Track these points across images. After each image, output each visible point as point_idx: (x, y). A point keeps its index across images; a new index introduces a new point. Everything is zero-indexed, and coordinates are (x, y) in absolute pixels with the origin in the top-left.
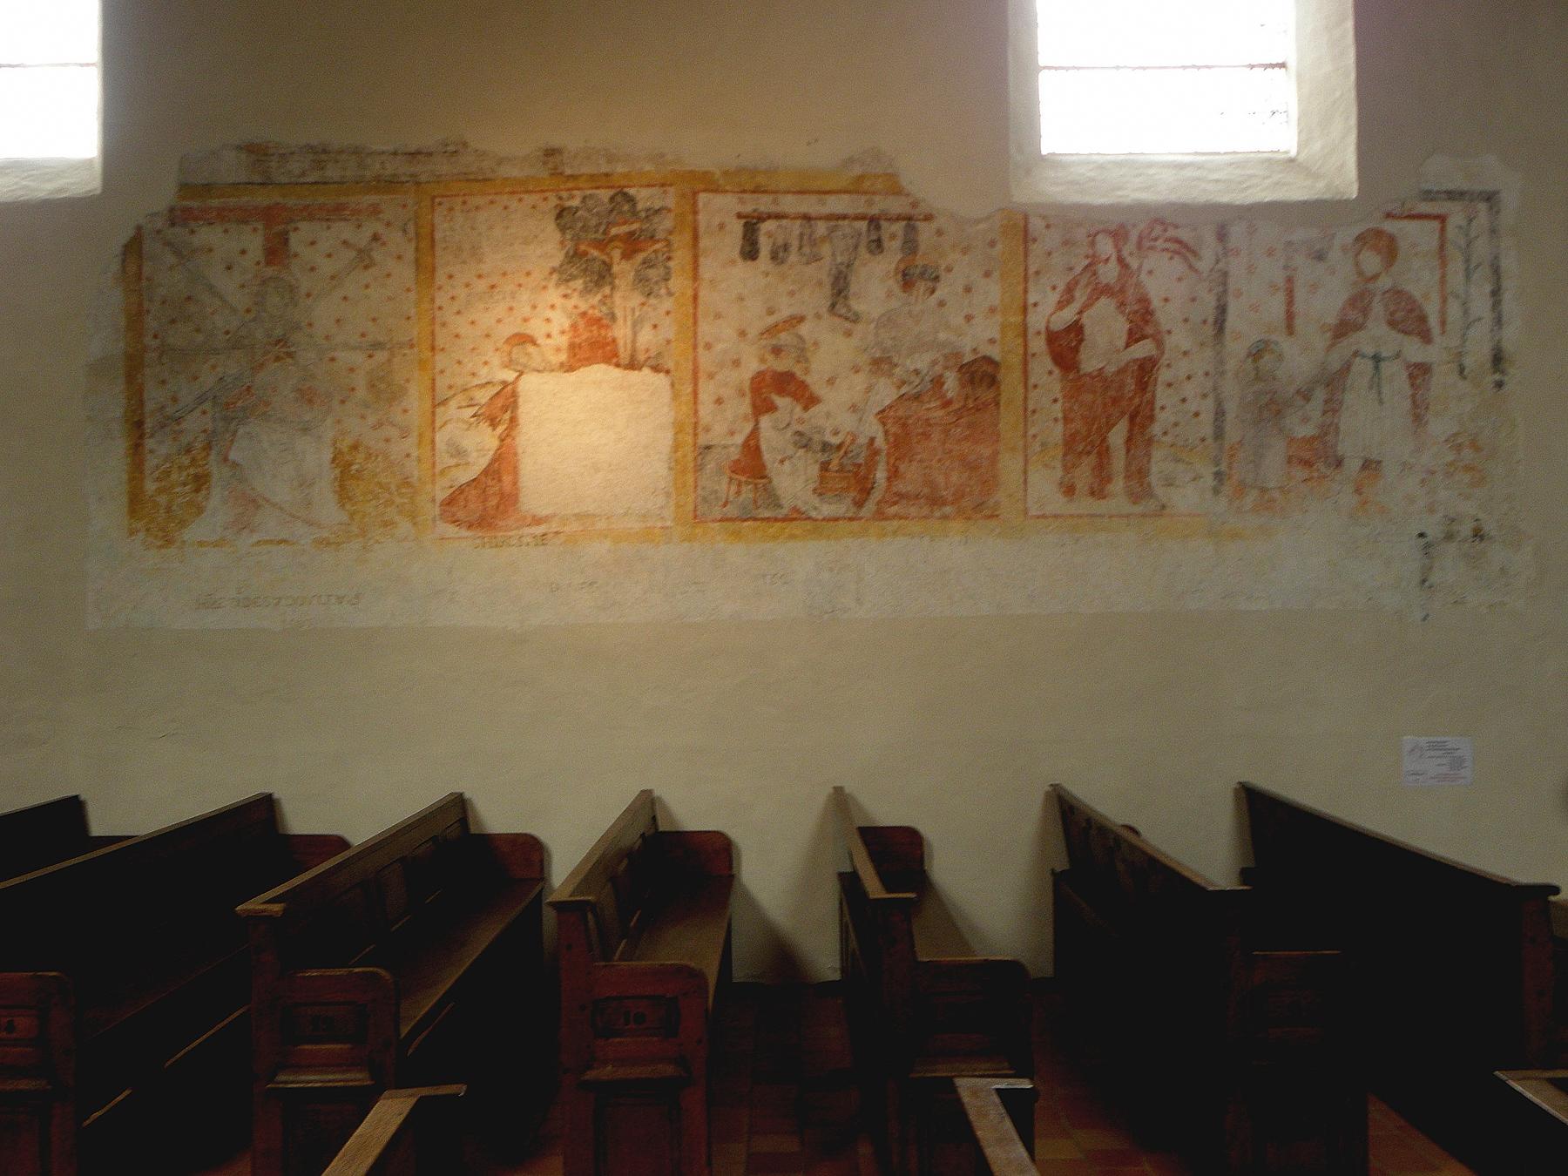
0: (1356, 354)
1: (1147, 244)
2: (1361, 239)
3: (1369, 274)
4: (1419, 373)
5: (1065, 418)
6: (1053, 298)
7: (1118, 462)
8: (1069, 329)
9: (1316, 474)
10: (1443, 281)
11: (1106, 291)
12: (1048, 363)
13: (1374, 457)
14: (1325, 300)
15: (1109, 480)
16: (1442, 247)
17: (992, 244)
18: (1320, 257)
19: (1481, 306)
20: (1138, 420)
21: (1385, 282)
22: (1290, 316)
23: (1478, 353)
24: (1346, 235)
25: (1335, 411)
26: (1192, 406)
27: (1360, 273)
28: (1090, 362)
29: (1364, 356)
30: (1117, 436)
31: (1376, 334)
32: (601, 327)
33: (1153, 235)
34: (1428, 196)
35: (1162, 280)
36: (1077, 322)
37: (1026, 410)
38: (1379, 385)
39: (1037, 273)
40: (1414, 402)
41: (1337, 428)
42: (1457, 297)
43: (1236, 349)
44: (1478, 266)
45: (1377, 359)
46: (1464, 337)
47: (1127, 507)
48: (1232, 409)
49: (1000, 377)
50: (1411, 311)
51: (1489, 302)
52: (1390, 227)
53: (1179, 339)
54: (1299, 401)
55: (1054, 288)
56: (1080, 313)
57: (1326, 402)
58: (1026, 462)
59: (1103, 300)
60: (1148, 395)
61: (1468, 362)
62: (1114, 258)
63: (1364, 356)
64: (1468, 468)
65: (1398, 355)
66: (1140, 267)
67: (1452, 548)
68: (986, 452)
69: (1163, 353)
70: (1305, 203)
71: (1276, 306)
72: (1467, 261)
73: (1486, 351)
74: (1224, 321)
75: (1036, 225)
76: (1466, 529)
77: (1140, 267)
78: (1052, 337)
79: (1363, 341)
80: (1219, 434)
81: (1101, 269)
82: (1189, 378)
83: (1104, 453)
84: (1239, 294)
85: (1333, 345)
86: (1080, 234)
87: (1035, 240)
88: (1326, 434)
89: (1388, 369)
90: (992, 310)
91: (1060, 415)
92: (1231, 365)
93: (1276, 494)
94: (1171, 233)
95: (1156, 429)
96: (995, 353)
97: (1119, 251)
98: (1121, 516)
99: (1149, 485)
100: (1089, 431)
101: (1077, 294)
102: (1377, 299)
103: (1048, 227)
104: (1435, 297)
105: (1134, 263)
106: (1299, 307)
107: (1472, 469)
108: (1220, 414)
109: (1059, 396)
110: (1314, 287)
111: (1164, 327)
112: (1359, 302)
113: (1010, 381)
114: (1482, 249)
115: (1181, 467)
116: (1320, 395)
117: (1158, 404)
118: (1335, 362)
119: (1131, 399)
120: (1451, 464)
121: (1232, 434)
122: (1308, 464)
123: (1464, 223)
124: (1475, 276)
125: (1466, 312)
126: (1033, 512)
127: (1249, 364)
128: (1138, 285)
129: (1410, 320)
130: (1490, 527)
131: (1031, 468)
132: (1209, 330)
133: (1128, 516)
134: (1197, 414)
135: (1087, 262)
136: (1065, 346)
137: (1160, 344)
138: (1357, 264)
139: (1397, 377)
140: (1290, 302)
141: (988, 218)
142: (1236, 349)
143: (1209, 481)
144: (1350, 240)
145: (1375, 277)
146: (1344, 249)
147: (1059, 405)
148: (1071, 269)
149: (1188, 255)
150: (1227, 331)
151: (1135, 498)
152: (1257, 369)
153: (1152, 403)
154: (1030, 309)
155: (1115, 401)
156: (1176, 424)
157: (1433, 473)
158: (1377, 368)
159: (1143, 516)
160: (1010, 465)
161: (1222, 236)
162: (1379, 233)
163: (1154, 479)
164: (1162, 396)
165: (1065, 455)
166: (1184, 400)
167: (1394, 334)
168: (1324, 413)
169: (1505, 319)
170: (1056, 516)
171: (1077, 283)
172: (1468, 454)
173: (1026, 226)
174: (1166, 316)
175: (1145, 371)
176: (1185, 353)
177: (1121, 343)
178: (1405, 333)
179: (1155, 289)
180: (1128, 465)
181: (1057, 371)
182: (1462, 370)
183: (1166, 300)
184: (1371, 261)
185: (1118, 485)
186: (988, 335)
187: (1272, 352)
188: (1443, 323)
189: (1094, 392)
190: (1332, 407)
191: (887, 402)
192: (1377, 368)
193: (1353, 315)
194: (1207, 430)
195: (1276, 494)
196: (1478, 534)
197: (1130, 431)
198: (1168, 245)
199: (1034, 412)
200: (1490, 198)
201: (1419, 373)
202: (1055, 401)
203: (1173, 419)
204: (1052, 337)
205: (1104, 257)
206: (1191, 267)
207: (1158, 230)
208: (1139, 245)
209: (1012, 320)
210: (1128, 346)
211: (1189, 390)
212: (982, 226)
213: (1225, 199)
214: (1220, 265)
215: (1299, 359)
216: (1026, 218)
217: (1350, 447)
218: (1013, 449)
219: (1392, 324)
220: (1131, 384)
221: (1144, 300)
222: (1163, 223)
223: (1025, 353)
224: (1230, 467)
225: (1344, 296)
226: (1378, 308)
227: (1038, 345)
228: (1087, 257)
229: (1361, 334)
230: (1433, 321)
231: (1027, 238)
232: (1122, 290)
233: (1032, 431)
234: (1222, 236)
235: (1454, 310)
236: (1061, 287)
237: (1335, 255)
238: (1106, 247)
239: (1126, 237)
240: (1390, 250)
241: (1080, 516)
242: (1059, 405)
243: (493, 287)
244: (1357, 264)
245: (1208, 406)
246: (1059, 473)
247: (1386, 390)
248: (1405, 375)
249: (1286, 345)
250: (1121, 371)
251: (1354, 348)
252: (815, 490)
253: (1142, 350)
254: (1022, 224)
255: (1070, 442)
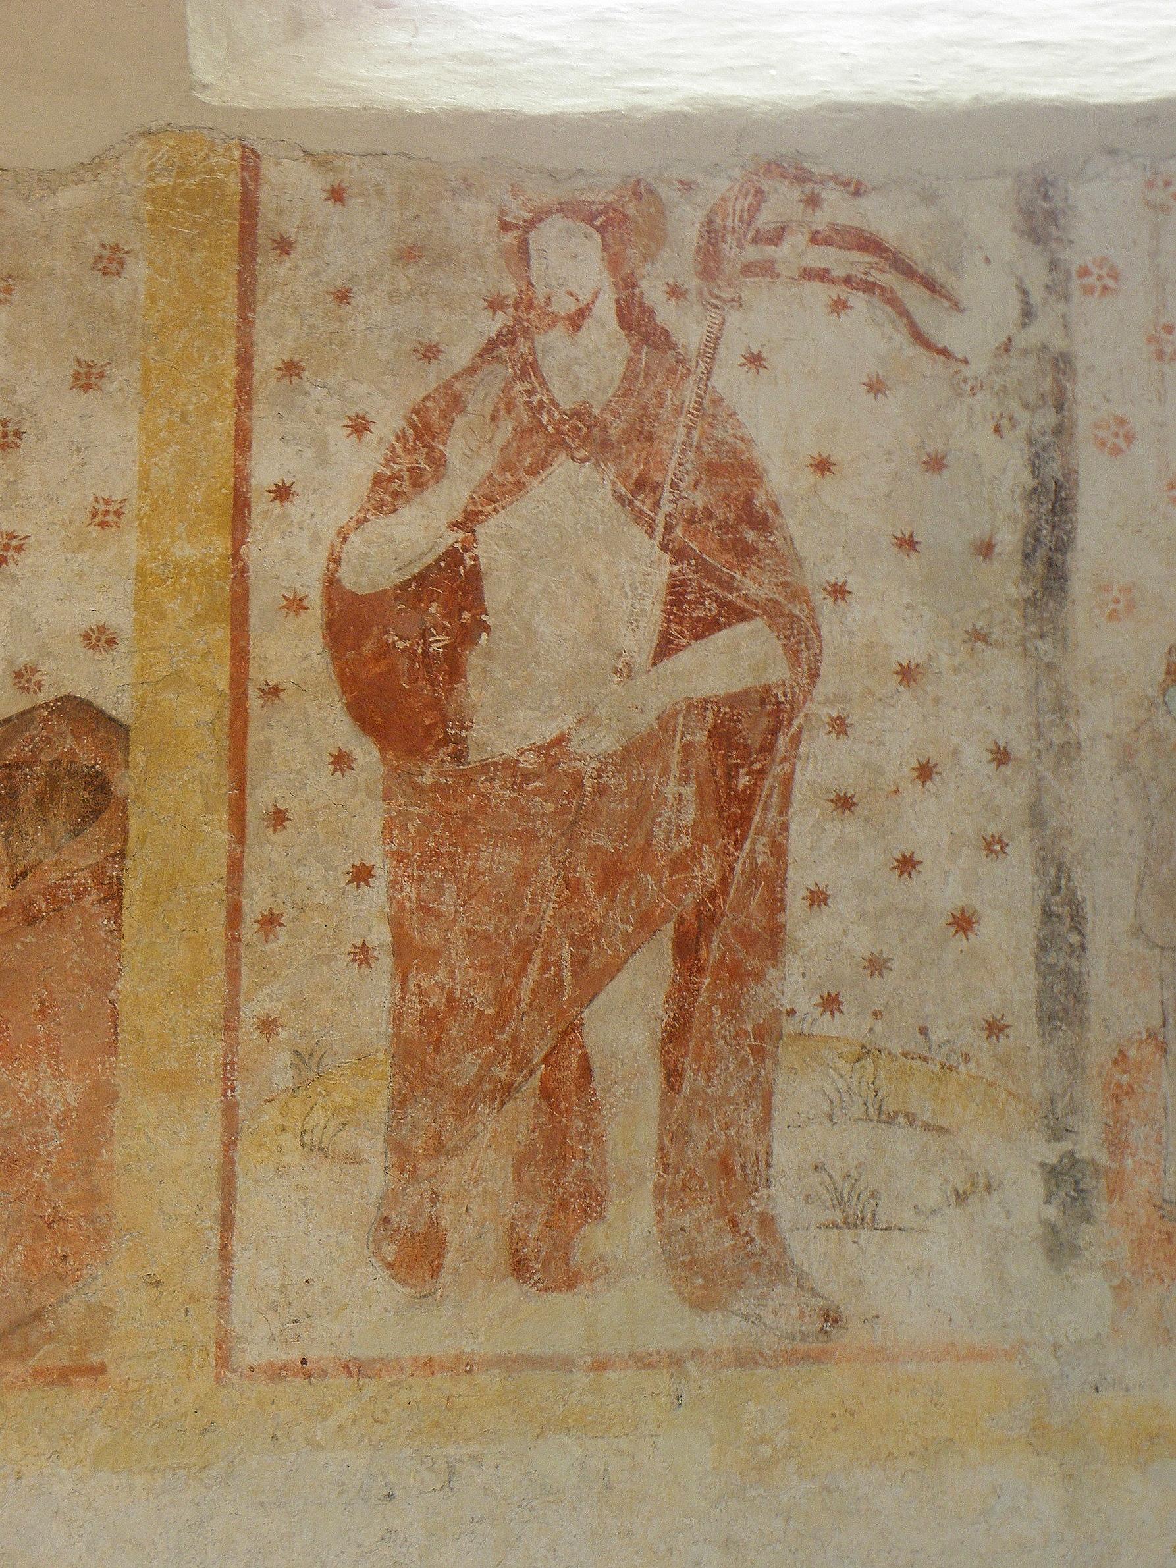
1: (735, 253)
5: (401, 947)
7: (631, 1124)
11: (580, 434)
12: (336, 726)
15: (592, 1202)
17: (111, 262)
20: (712, 952)
26: (943, 888)
28: (506, 712)
30: (625, 1021)
32: (508, 411)
33: (765, 219)
35: (798, 388)
36: (453, 556)
37: (235, 915)
39: (291, 369)
47: (672, 1325)
49: (123, 784)
53: (878, 617)
55: (359, 426)
56: (468, 522)
58: (230, 1143)
59: (562, 469)
60: (757, 846)
62: (605, 308)
66: (715, 340)
68: (62, 1094)
69: (814, 676)
74: (1062, 546)
75: (290, 186)
78: (349, 621)
80: (1062, 1001)
81: (555, 349)
82: (925, 772)
83: (567, 1087)
86: (471, 222)
87: (284, 246)
90: (105, 516)
91: (380, 936)
92: (1101, 717)
94: (838, 209)
95: (792, 986)
96: (110, 685)
97: (629, 284)
98: (644, 1362)
99: (767, 1222)
100: (504, 999)
101: (455, 449)
103: (337, 195)
105: (688, 328)
108: (1061, 918)
109: (377, 857)
111: (817, 573)
113: (171, 802)
115: (903, 1143)
117: (799, 881)
119: (680, 864)
126: (256, 1349)
128: (709, 409)
131: (245, 1154)
132: (1006, 582)
133: (675, 1361)
134: (963, 923)
135: (495, 324)
136: (405, 658)
137: (800, 639)
141: (94, 166)
143: (1027, 1202)
147: (377, 892)
148: (430, 353)
149: (912, 295)
150: (1080, 585)
151: (704, 1281)
153: (771, 882)
154: (260, 505)
155: (612, 874)
156: (876, 965)
159: (746, 1359)
160: (161, 1149)
161: (1041, 217)
163: (786, 1199)
164: (815, 850)
165: (400, 1102)
166: (907, 864)
170: (355, 1369)
171: (456, 403)
173: (249, 208)
174: (823, 530)
175: (741, 750)
176: (907, 674)
177: (638, 641)
179: (774, 425)
180: (674, 1135)
181: (367, 754)
183: (823, 466)
185: (630, 1227)
186: (82, 616)
189: (527, 838)
194: (1012, 985)
197: (682, 998)
198: (818, 257)
199: (270, 921)
202: (362, 875)
203: (862, 943)
204: (349, 621)
205: (563, 305)
206: (919, 338)
207: (783, 201)
209: (184, 551)
210: (666, 648)
211: (927, 822)
212: (65, 198)
214: (1037, 332)
216: (250, 162)
218: (175, 1083)
220: (680, 803)
221: (734, 469)
222: (802, 177)
223: (239, 683)
227: (293, 651)
228: (495, 305)
231: (252, 236)
232: (642, 433)
233: (253, 1008)
234: (1041, 217)
236: (388, 422)
238: (573, 266)
239: (656, 235)
241: (466, 1367)
242: (377, 892)
245: (1014, 883)
246: (376, 1178)
250: (640, 750)
254: (233, 185)
255: (418, 1053)
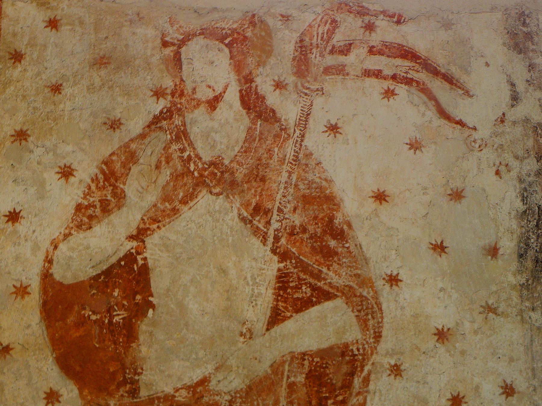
1: (318, 60)
6: (65, 197)
8: (106, 278)
11: (216, 177)
33: (338, 39)
36: (130, 258)
53: (421, 298)
56: (140, 235)
59: (204, 200)
62: (233, 96)
66: (306, 116)
69: (378, 336)
77: (306, 116)
78: (58, 301)
81: (199, 122)
94: (386, 32)
97: (248, 80)
101: (131, 187)
103: (53, 24)
105: (288, 109)
111: (379, 267)
128: (302, 160)
135: (158, 106)
137: (368, 312)
148: (115, 125)
149: (437, 86)
171: (132, 158)
174: (382, 240)
176: (442, 335)
177: (257, 313)
179: (347, 169)
183: (381, 197)
191: (245, 135)
198: (387, 65)
204: (58, 301)
206: (443, 113)
208: (302, 63)
210: (276, 318)
221: (321, 199)
228: (158, 94)
232: (258, 176)
236: (86, 169)
238: (211, 69)
239: (266, 49)
252: (346, 55)
253: (320, 327)
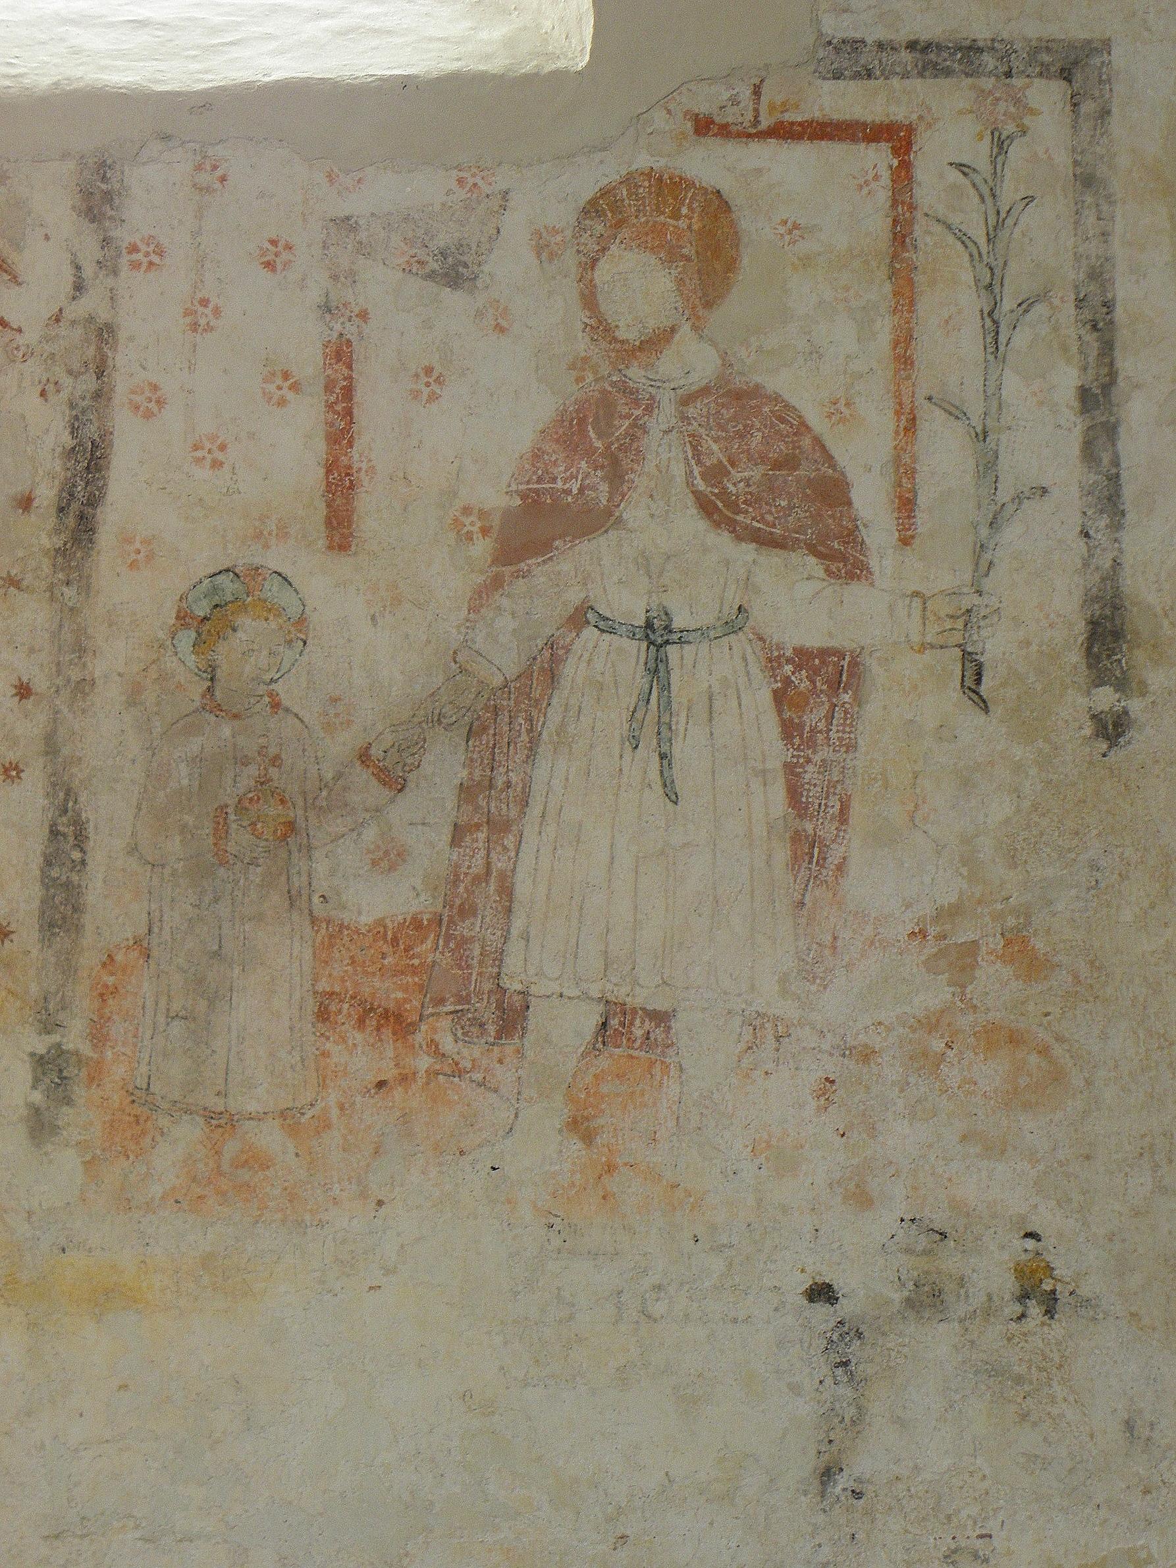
0: (579, 618)
2: (605, 209)
3: (628, 333)
4: (816, 686)
9: (424, 1062)
10: (903, 355)
13: (644, 996)
14: (471, 421)
16: (901, 236)
18: (454, 272)
19: (1043, 441)
21: (692, 361)
22: (340, 484)
23: (1034, 611)
24: (549, 198)
25: (499, 827)
27: (601, 329)
29: (607, 626)
31: (660, 544)
34: (849, 58)
38: (664, 730)
40: (794, 794)
41: (507, 891)
42: (956, 413)
43: (134, 598)
44: (1026, 305)
45: (657, 635)
46: (982, 561)
48: (111, 815)
50: (788, 463)
51: (1074, 428)
52: (708, 165)
54: (365, 789)
57: (467, 792)
61: (996, 645)
63: (607, 626)
64: (1002, 1038)
65: (736, 621)
67: (938, 1341)
70: (406, 85)
71: (292, 446)
72: (991, 287)
73: (1062, 608)
76: (991, 1271)
79: (604, 574)
80: (62, 911)
84: (152, 403)
85: (497, 583)
88: (466, 911)
89: (696, 670)
92: (114, 657)
93: (270, 1138)
102: (666, 414)
104: (878, 421)
106: (374, 445)
107: (1015, 1039)
108: (67, 836)
110: (430, 380)
112: (598, 429)
114: (1045, 240)
116: (445, 766)
118: (502, 654)
120: (931, 1023)
121: (112, 907)
122: (395, 1022)
123: (979, 154)
124: (1021, 339)
125: (988, 467)
127: (183, 659)
129: (787, 497)
130: (1075, 1262)
138: (589, 300)
139: (726, 692)
140: (341, 431)
142: (134, 598)
144: (563, 216)
145: (655, 342)
146: (543, 248)
150: (106, 537)
152: (211, 674)
157: (867, 1055)
158: (657, 669)
161: (98, 200)
162: (669, 188)
167: (722, 541)
168: (458, 834)
169: (1128, 491)
172: (994, 981)
178: (765, 541)
182: (973, 675)
184: (640, 286)
187: (270, 609)
188: (906, 505)
190: (489, 812)
192: (657, 669)
193: (575, 478)
195: (270, 1138)
196: (1037, 1290)
200: (1073, 66)
201: (816, 686)
213: (123, 76)
215: (367, 640)
217: (553, 962)
219: (716, 509)
224: (98, 1035)
225: (541, 408)
226: (664, 456)
229: (603, 543)
230: (870, 500)
234: (98, 200)
235: (945, 454)
237: (510, 265)
240: (708, 243)
243: (56, 383)
244: (589, 300)
247: (689, 748)
248: (760, 696)
249: (326, 590)
251: (574, 596)
252: (330, 548)
